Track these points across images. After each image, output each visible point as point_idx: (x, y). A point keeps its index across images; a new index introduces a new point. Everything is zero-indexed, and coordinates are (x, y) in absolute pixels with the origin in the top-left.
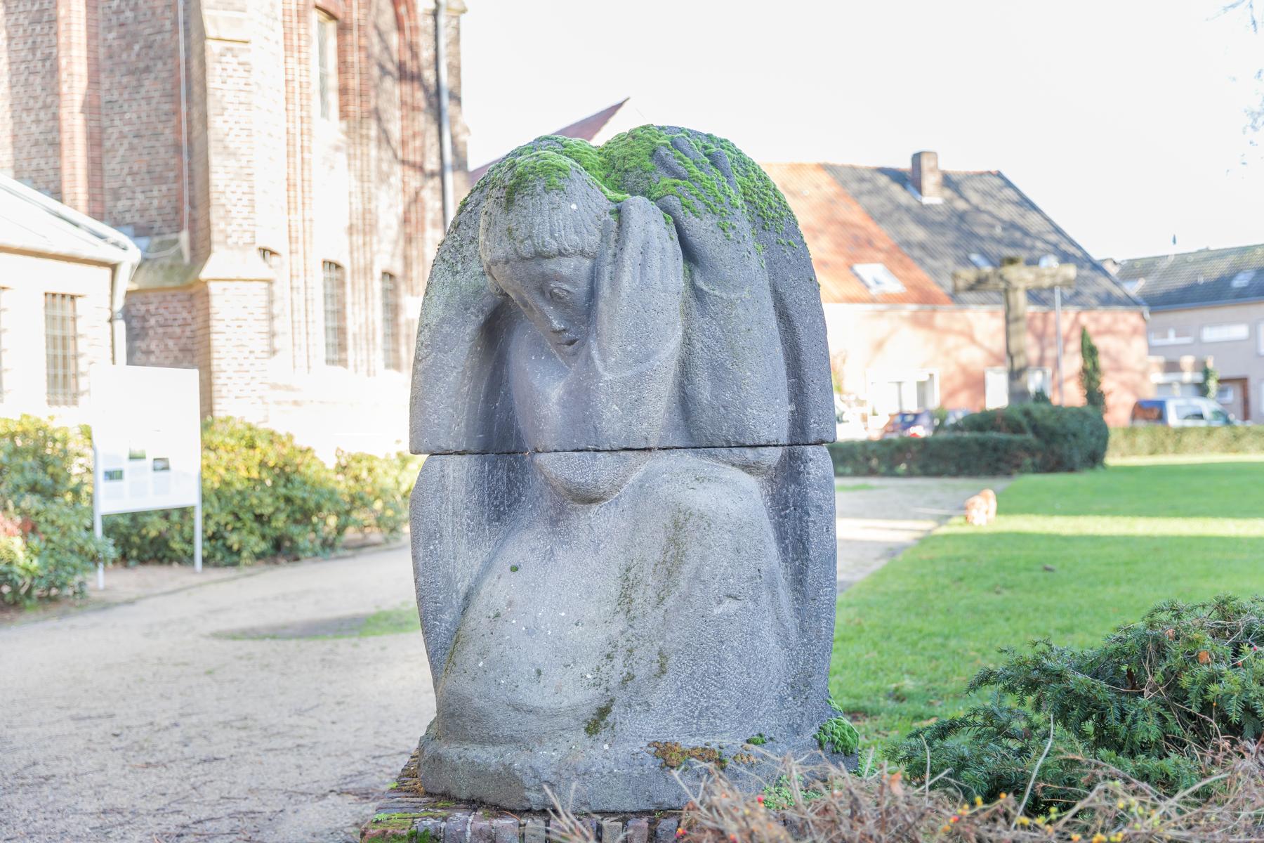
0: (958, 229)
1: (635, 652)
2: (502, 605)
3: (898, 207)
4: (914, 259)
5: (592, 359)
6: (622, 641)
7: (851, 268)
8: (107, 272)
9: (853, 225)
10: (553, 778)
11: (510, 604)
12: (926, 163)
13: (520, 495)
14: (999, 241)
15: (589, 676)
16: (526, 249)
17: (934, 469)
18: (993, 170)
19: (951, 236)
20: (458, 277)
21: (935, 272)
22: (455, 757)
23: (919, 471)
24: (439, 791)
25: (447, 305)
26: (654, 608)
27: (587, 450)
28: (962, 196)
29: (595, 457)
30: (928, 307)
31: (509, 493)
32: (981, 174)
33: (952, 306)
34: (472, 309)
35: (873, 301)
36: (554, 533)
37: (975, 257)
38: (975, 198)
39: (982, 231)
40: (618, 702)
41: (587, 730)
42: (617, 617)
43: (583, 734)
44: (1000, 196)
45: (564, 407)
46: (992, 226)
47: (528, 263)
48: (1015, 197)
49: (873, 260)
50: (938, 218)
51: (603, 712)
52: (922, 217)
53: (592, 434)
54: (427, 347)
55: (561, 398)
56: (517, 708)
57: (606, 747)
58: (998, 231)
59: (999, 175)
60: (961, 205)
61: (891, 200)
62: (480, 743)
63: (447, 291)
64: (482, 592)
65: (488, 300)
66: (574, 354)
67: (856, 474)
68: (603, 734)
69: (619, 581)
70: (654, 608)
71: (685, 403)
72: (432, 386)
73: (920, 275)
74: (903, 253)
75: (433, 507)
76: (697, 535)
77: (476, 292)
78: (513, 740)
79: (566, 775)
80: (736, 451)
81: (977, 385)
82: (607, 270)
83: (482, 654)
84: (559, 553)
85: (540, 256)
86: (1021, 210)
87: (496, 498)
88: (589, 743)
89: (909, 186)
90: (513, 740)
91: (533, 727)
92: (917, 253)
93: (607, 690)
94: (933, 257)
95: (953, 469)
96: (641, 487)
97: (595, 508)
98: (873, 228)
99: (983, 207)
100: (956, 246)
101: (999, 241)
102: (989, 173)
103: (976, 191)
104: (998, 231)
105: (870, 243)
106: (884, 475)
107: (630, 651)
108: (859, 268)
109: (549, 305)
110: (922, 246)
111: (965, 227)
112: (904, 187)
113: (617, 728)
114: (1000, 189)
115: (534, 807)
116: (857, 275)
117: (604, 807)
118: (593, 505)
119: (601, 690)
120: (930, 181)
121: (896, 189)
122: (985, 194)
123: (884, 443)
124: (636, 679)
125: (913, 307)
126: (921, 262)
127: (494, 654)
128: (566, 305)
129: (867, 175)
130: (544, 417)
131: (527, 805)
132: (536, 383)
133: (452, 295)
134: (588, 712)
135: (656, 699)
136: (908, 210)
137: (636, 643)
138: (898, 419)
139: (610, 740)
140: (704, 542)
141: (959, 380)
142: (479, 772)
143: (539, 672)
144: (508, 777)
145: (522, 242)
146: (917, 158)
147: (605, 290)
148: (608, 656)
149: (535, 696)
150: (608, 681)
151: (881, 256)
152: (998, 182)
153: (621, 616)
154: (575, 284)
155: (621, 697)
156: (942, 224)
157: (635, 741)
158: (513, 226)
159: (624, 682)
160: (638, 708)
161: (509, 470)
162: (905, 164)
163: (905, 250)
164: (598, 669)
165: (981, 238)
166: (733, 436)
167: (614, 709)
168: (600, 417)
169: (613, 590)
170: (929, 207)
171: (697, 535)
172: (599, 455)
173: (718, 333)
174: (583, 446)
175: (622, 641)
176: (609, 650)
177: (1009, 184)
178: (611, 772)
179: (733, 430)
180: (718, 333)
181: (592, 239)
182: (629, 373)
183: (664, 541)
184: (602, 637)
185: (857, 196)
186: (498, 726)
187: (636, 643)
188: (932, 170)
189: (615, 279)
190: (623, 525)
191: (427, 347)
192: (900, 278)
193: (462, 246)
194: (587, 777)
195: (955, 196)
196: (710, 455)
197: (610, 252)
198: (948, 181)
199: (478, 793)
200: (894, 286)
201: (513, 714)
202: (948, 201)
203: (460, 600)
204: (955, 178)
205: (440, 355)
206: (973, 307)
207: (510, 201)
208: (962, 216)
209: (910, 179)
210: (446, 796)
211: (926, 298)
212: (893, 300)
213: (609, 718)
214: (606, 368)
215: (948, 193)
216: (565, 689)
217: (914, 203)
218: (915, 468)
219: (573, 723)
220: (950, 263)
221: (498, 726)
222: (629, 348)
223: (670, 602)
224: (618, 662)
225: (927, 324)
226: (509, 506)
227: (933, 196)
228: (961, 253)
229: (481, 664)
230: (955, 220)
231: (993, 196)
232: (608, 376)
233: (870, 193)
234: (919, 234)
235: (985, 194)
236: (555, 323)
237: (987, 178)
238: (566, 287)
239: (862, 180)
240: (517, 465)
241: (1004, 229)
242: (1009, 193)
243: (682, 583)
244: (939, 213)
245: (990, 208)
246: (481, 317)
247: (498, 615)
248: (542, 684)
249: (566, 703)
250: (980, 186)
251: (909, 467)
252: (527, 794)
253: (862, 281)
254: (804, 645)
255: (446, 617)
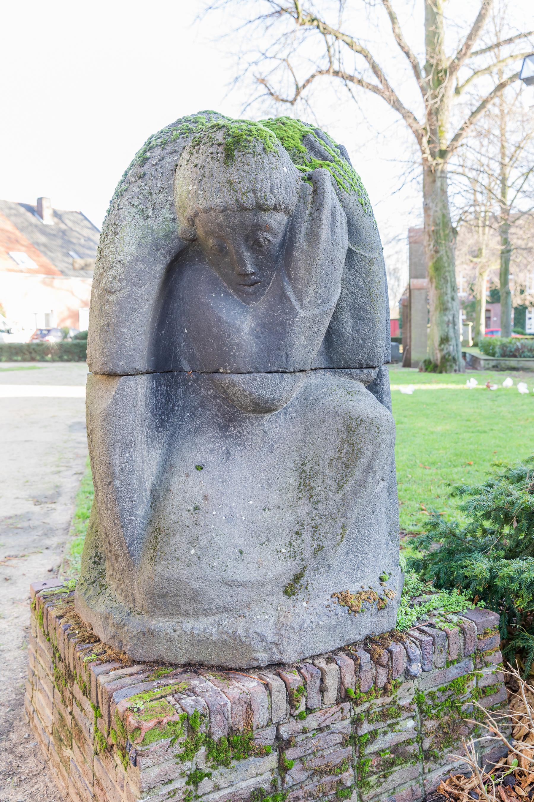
0: (62, 238)
1: (320, 528)
2: (199, 500)
3: (31, 224)
4: (41, 251)
5: (288, 299)
6: (307, 521)
7: (8, 254)
8: (290, 98)
9: (7, 231)
10: (276, 639)
11: (206, 498)
12: (45, 204)
13: (174, 405)
14: (83, 246)
15: (283, 550)
16: (248, 201)
17: (65, 357)
18: (78, 211)
19: (59, 242)
20: (149, 221)
21: (52, 259)
22: (169, 631)
23: (58, 359)
24: (151, 659)
25: (140, 245)
26: (334, 494)
27: (277, 372)
28: (63, 222)
29: (282, 377)
30: (50, 276)
31: (167, 404)
32: (72, 212)
33: (62, 277)
34: (162, 251)
35: (21, 271)
36: (226, 437)
37: (72, 253)
38: (70, 224)
39: (74, 241)
40: (309, 568)
41: (285, 593)
42: (301, 502)
43: (282, 597)
44: (82, 224)
45: (257, 337)
46: (79, 239)
47: (246, 213)
48: (89, 225)
49: (19, 250)
50: (52, 232)
51: (297, 578)
52: (43, 230)
53: (284, 359)
54: (120, 281)
55: (253, 330)
56: (229, 584)
57: (305, 604)
58: (82, 241)
59: (81, 213)
60: (63, 227)
61: (27, 220)
62: (194, 616)
63: (140, 233)
64: (174, 489)
65: (176, 243)
66: (254, 293)
67: (24, 360)
68: (300, 595)
69: (296, 473)
70: (334, 494)
71: (332, 337)
72: (127, 315)
73: (44, 259)
74: (34, 248)
75: (130, 421)
76: (370, 436)
77: (167, 236)
78: (226, 609)
79: (286, 634)
80: (365, 371)
81: (75, 316)
82: (304, 226)
83: (193, 542)
84: (236, 452)
85: (260, 208)
86: (93, 232)
87: (160, 409)
88: (290, 603)
89: (36, 214)
90: (226, 609)
91: (243, 597)
92: (42, 248)
93: (302, 560)
94: (51, 251)
95: (77, 358)
96: (306, 399)
97: (267, 416)
98: (18, 233)
99: (74, 228)
100: (62, 247)
101: (83, 246)
102: (76, 212)
103: (70, 220)
104: (82, 241)
105: (17, 241)
106: (39, 361)
107: (316, 527)
108: (12, 253)
109: (248, 251)
110: (45, 245)
111: (66, 238)
112: (33, 214)
113: (310, 588)
114: (82, 221)
115: (263, 665)
116: (11, 258)
117: (314, 653)
118: (266, 415)
119: (298, 560)
120: (47, 213)
121: (29, 215)
122: (74, 222)
123: (28, 346)
124: (324, 550)
125: (44, 276)
126: (45, 254)
127: (203, 541)
128: (262, 253)
129: (13, 206)
130: (237, 345)
131: (255, 664)
132: (223, 315)
133: (144, 237)
134: (286, 580)
135: (334, 562)
136: (36, 226)
137: (319, 521)
138: (39, 332)
139: (306, 598)
140: (375, 441)
141: (66, 313)
142: (195, 641)
143: (241, 552)
144: (235, 642)
145: (245, 194)
146: (40, 200)
147: (302, 241)
148: (297, 533)
149: (241, 572)
150: (302, 553)
151: (23, 249)
152: (80, 217)
153: (304, 501)
154: (275, 236)
155: (312, 563)
156: (54, 235)
157: (323, 596)
158: (235, 178)
159: (315, 553)
160: (323, 570)
161: (168, 386)
162: (34, 203)
163: (36, 247)
164: (290, 544)
165: (74, 244)
166: (366, 361)
167: (306, 574)
168: (291, 345)
169: (291, 480)
170: (47, 226)
171: (370, 436)
172: (285, 376)
173: (361, 283)
174: (275, 368)
175: (307, 521)
176: (297, 528)
177: (86, 219)
178: (318, 624)
179: (366, 356)
180: (361, 283)
181: (292, 199)
182: (317, 311)
183: (338, 442)
184: (291, 519)
185: (9, 216)
186: (212, 600)
187: (319, 521)
188: (48, 207)
189: (313, 235)
190: (294, 429)
191: (120, 281)
192: (34, 260)
193: (151, 194)
194: (302, 633)
195: (60, 221)
196: (346, 374)
197: (307, 211)
198: (56, 214)
199: (197, 658)
200: (34, 265)
201: (225, 590)
202: (56, 224)
203: (148, 496)
204: (59, 213)
205: (135, 289)
206: (73, 278)
207: (229, 156)
208: (64, 232)
209: (36, 211)
210: (160, 663)
211: (49, 272)
212: (31, 271)
213: (302, 581)
214: (302, 306)
215: (56, 220)
216: (265, 563)
217: (38, 223)
218: (56, 358)
219: (275, 588)
220: (59, 255)
221: (212, 600)
222: (320, 291)
223: (347, 488)
224: (307, 536)
225: (50, 285)
226: (167, 415)
227: (48, 220)
228: (65, 251)
229: (193, 552)
230: (61, 234)
231: (78, 224)
232: (303, 313)
233: (15, 215)
234: (43, 239)
235: (74, 222)
236: (249, 267)
237: (75, 214)
238: (269, 237)
239: (11, 208)
240: (173, 381)
241: (85, 240)
242: (86, 222)
243: (357, 473)
244: (52, 230)
245: (77, 229)
246: (168, 258)
247: (196, 509)
248: (245, 562)
249: (269, 575)
250: (72, 218)
251: (52, 356)
252: (256, 655)
253: (14, 261)
254: (391, 504)
255: (138, 512)
